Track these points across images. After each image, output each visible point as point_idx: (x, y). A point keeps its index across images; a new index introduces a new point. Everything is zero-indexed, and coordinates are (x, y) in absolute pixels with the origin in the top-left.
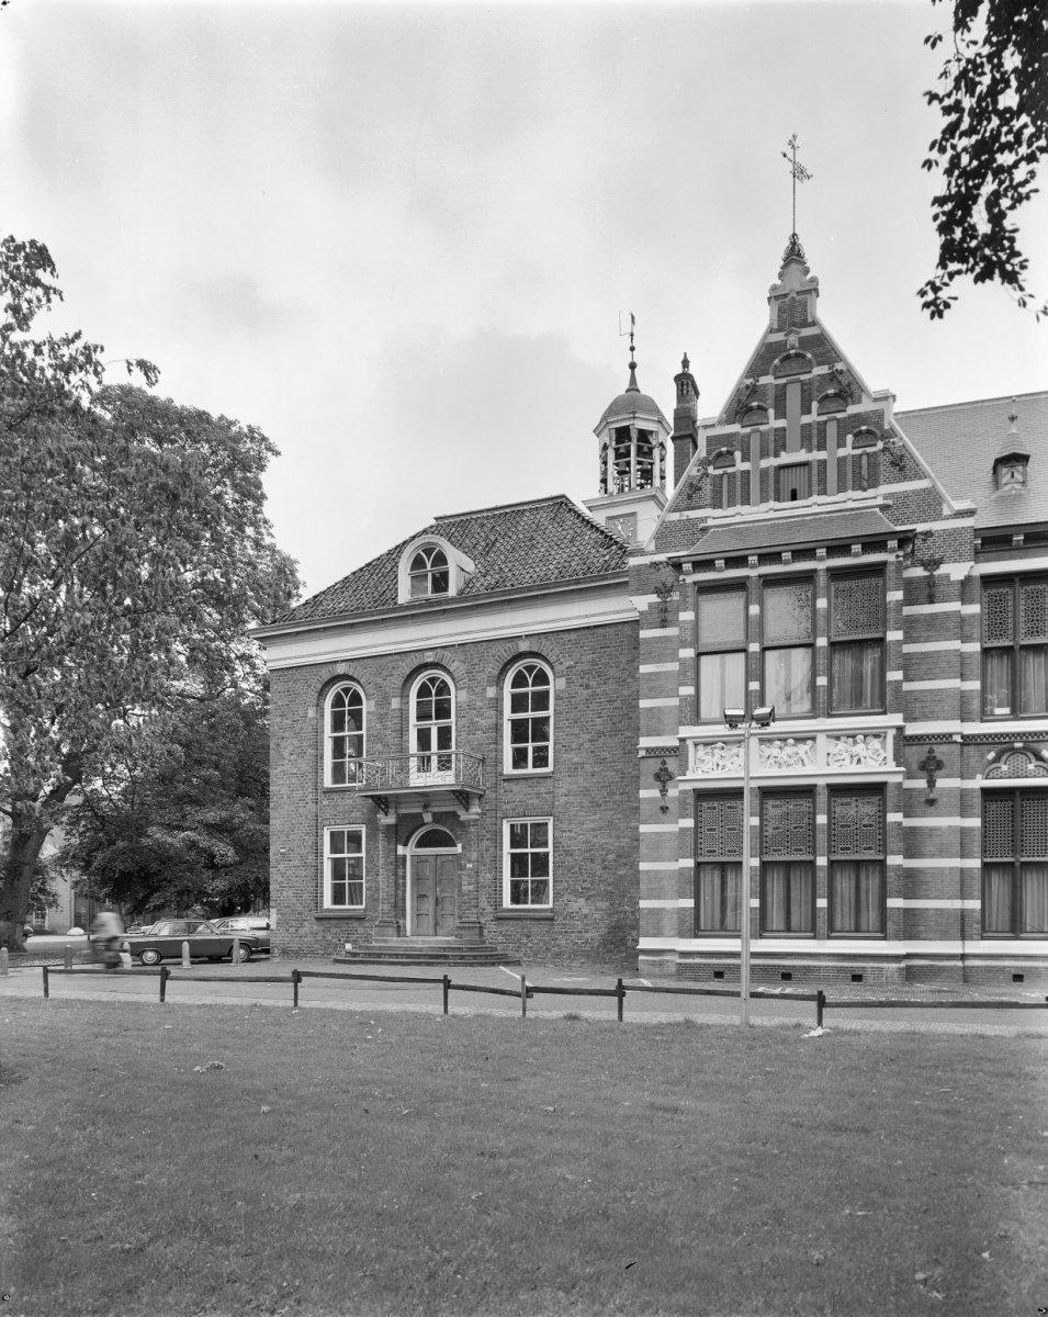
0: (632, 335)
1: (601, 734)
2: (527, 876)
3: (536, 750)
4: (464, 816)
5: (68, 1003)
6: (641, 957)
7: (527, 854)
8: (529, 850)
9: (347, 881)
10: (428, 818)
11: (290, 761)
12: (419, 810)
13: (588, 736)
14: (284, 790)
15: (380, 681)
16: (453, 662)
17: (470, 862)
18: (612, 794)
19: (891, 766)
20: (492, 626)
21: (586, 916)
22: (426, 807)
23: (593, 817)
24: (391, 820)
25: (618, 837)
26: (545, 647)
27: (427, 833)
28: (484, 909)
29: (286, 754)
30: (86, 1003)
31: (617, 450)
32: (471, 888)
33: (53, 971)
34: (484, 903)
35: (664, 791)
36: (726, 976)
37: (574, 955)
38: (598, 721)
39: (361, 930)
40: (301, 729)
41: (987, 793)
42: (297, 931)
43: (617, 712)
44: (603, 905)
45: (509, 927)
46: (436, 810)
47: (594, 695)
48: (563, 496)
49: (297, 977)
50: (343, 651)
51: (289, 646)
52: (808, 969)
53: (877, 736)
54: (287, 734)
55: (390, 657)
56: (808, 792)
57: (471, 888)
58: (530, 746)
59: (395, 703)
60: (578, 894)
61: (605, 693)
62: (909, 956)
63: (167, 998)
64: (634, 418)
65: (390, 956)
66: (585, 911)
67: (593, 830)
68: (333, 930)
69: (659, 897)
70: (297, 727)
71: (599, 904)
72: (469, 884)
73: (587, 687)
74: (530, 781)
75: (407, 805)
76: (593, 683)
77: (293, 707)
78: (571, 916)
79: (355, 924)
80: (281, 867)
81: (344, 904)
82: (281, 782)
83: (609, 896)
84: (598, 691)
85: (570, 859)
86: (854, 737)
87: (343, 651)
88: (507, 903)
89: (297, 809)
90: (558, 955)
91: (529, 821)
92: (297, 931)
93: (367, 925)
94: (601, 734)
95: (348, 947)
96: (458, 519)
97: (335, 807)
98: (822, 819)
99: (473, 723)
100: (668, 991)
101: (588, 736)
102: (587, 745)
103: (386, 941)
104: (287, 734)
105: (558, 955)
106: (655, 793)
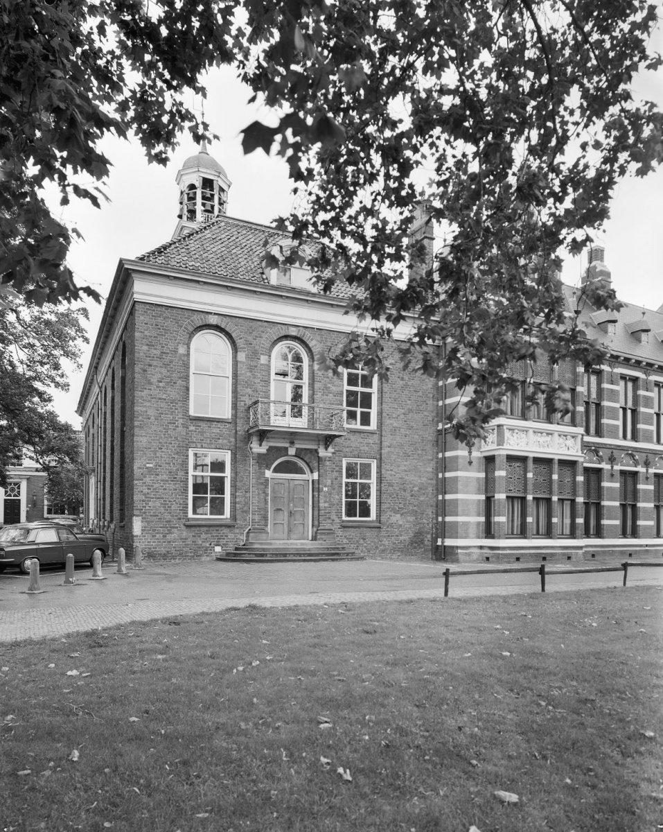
0: (203, 114)
1: (410, 411)
2: (356, 502)
3: (362, 413)
4: (322, 453)
5: (464, 601)
6: (459, 551)
7: (356, 483)
8: (358, 481)
9: (209, 496)
10: (292, 451)
11: (158, 387)
12: (287, 445)
13: (403, 411)
14: (151, 412)
15: (250, 338)
16: (312, 340)
17: (325, 486)
18: (416, 449)
19: (580, 453)
20: (335, 321)
21: (401, 526)
22: (292, 443)
23: (405, 463)
24: (263, 450)
25: (420, 477)
26: (307, 336)
27: (287, 462)
28: (333, 520)
29: (154, 380)
30: (490, 600)
31: (188, 194)
32: (326, 505)
33: (454, 574)
34: (334, 517)
35: (470, 452)
36: (521, 560)
37: (394, 550)
38: (409, 402)
39: (231, 536)
40: (171, 362)
41: (623, 473)
42: (164, 536)
43: (419, 399)
44: (411, 519)
45: (351, 533)
46: (298, 446)
47: (406, 385)
48: (614, 292)
49: (625, 567)
50: (218, 306)
51: (163, 286)
52: (552, 555)
53: (573, 437)
54: (154, 363)
55: (259, 323)
56: (524, 459)
57: (326, 505)
58: (359, 410)
59: (263, 359)
60: (396, 512)
61: (412, 385)
62: (587, 546)
63: (546, 587)
64: (219, 176)
65: (294, 555)
66: (401, 523)
67: (406, 471)
68: (203, 536)
69: (467, 515)
70: (167, 359)
71: (409, 518)
72: (325, 502)
73: (403, 379)
74: (362, 434)
75: (273, 440)
76: (406, 378)
77: (162, 340)
78: (391, 525)
79: (226, 531)
80: (147, 480)
81: (355, 516)
82: (148, 404)
83: (415, 513)
84: (410, 383)
85: (391, 488)
86: (566, 436)
87: (218, 306)
88: (190, 515)
89: (167, 430)
90: (383, 551)
91: (359, 461)
92: (164, 536)
93: (237, 531)
94: (410, 411)
95: (218, 549)
96: (242, 224)
97: (202, 433)
98: (555, 477)
99: (327, 388)
100: (498, 571)
101: (403, 411)
102: (402, 416)
103: (271, 544)
104: (154, 363)
105: (383, 551)
106: (465, 453)
